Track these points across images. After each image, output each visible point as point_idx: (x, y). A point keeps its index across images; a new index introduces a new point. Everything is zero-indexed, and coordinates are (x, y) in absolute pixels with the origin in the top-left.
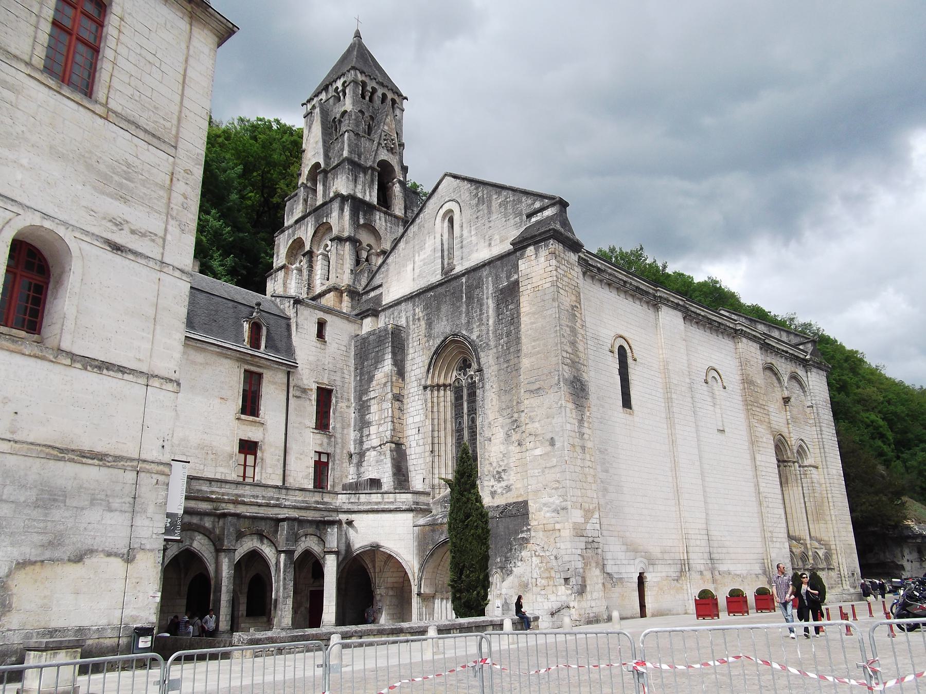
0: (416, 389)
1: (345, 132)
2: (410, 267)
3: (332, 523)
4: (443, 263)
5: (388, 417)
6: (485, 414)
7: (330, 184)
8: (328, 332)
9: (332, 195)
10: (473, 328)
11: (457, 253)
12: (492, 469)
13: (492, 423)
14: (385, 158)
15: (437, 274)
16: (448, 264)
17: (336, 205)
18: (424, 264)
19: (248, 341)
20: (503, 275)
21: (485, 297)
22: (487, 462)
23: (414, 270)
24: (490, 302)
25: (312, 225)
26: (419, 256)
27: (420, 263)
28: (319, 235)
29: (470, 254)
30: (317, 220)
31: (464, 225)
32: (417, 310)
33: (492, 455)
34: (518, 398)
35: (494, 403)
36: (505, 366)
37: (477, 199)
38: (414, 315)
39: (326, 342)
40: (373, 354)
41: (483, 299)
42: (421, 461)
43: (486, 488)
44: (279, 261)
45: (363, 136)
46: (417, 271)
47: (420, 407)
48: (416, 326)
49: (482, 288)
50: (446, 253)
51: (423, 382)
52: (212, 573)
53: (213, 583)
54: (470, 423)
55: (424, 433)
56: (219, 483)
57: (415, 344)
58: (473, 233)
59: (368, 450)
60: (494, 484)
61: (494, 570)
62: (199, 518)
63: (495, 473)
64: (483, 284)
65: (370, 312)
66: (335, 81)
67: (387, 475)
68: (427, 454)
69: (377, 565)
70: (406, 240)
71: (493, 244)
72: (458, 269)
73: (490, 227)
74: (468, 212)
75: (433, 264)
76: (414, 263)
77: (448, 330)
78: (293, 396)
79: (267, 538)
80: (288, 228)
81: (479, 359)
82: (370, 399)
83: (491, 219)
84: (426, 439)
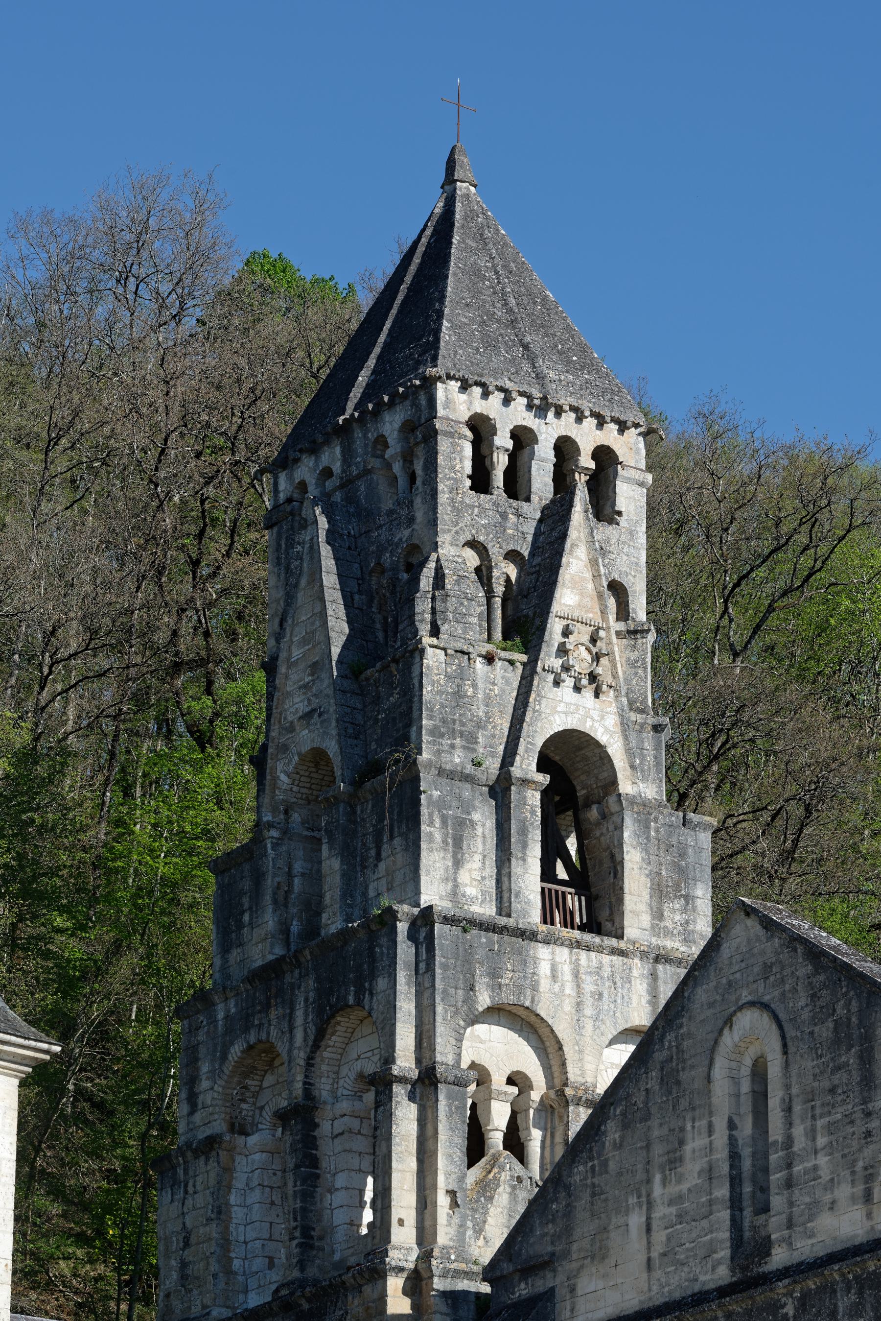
2: (636, 1220)
4: (736, 1225)
11: (777, 1201)
15: (719, 1262)
26: (664, 1183)
31: (797, 1108)
37: (831, 1025)
44: (198, 1118)
46: (660, 1237)
50: (747, 1189)
58: (821, 1141)
72: (779, 1257)
83: (870, 1106)
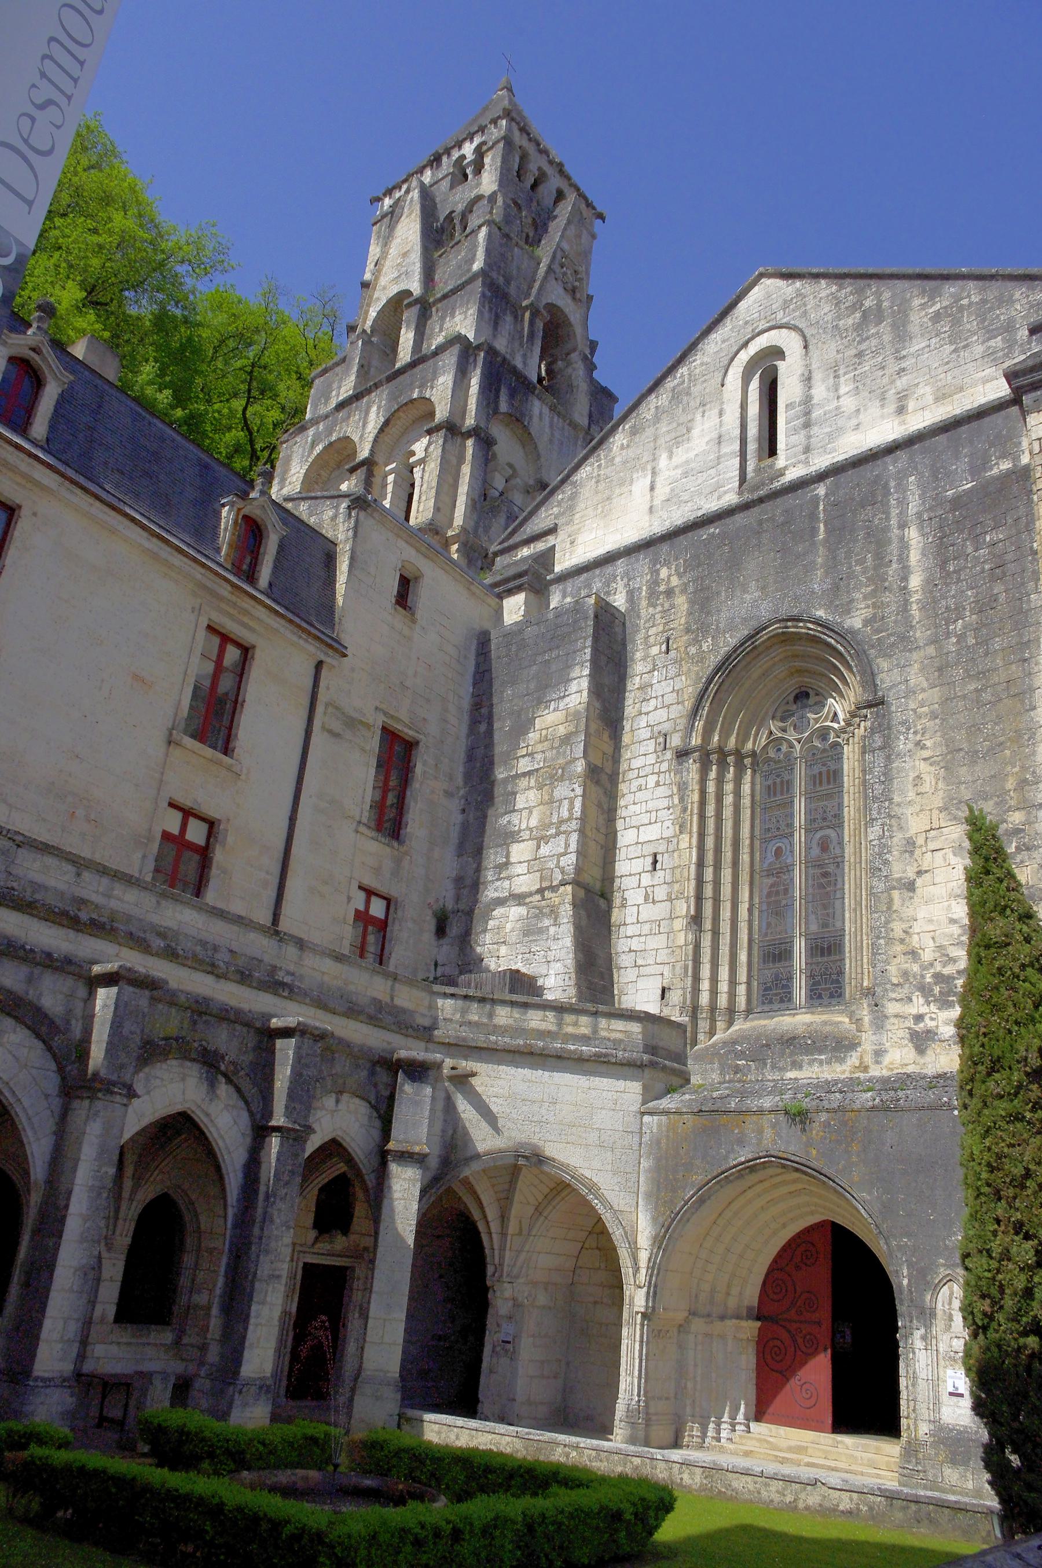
0: (651, 759)
1: (480, 227)
2: (641, 484)
3: (418, 1071)
5: (570, 819)
6: (890, 816)
7: (433, 329)
8: (423, 597)
9: (439, 339)
10: (852, 601)
12: (915, 968)
13: (920, 841)
14: (560, 303)
16: (758, 470)
17: (450, 360)
18: (686, 474)
19: (227, 555)
20: (961, 465)
21: (894, 522)
22: (898, 948)
23: (652, 488)
24: (913, 534)
25: (379, 408)
26: (670, 457)
27: (673, 473)
28: (393, 430)
29: (831, 437)
30: (392, 398)
31: (817, 376)
32: (664, 573)
33: (916, 928)
34: (1024, 768)
35: (926, 787)
36: (972, 687)
37: (858, 315)
38: (656, 582)
39: (414, 621)
40: (534, 668)
41: (887, 529)
42: (658, 942)
43: (892, 1020)
45: (517, 244)
47: (665, 803)
48: (659, 608)
49: (886, 505)
51: (676, 741)
52: (38, 1170)
53: (34, 1199)
54: (816, 851)
55: (673, 869)
56: (105, 881)
57: (655, 650)
58: (843, 389)
59: (501, 902)
60: (924, 1010)
61: (943, 1272)
62: (24, 970)
63: (928, 979)
64: (887, 493)
65: (525, 579)
66: (459, 145)
67: (557, 967)
68: (679, 924)
69: (513, 1212)
70: (633, 427)
71: (911, 408)
73: (904, 370)
74: (828, 350)
75: (712, 472)
76: (654, 473)
77: (765, 611)
78: (323, 728)
79: (229, 1081)
80: (315, 421)
81: (873, 675)
82: (517, 776)
84: (676, 886)
